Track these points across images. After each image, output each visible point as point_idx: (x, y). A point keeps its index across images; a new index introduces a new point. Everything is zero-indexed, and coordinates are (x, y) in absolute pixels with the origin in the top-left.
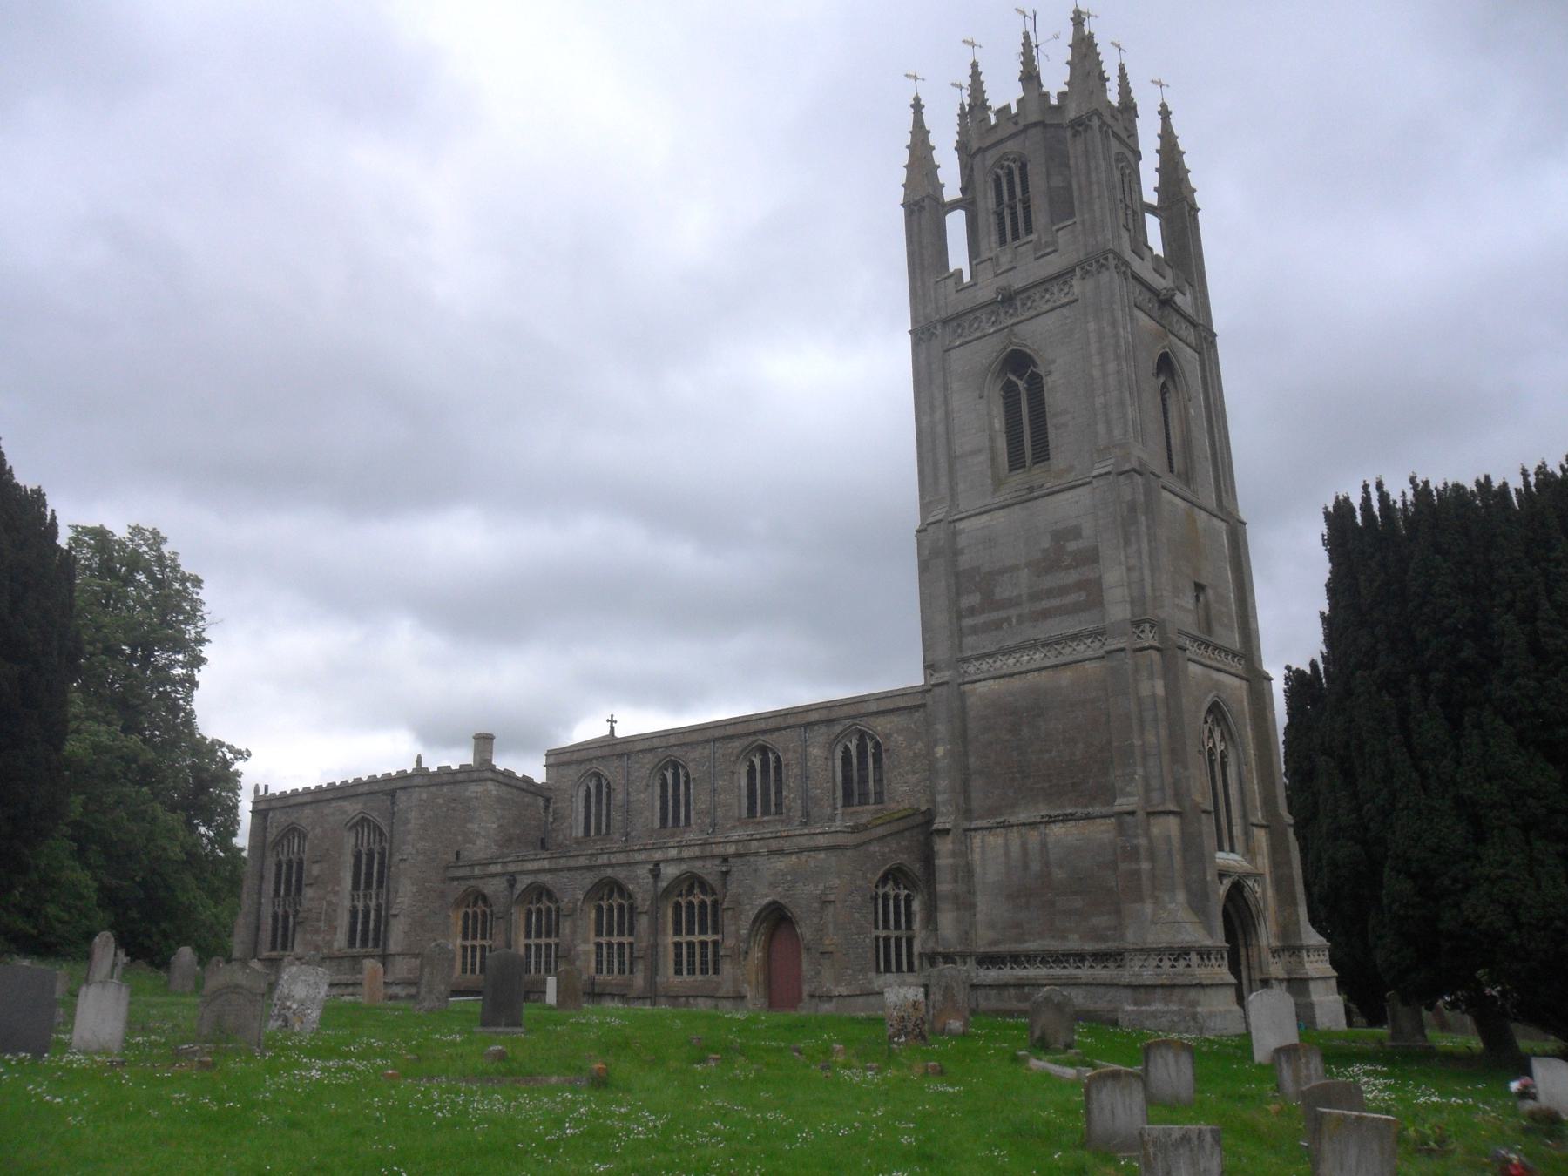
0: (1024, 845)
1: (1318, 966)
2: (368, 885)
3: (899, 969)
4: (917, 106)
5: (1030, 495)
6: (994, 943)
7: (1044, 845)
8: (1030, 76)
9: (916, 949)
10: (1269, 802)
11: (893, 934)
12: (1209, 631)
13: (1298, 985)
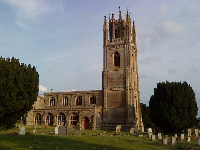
0: (114, 110)
4: (105, 17)
5: (117, 70)
8: (120, 17)
10: (139, 106)
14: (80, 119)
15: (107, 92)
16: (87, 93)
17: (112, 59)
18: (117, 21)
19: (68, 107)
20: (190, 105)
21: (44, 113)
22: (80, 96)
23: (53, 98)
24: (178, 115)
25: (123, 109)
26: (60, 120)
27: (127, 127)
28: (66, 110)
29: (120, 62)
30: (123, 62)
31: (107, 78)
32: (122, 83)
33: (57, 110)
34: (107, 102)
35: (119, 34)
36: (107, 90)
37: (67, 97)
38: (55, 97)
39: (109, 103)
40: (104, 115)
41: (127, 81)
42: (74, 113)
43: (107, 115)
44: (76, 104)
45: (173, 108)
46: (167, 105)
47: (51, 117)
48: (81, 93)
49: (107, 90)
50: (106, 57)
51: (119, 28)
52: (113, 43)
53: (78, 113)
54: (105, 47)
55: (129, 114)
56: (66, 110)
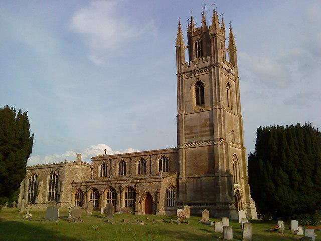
1: (253, 205)
2: (53, 188)
3: (171, 206)
4: (179, 24)
6: (191, 201)
7: (201, 182)
8: (204, 22)
9: (174, 202)
11: (170, 199)
12: (234, 140)
13: (249, 209)
14: (139, 197)
15: (183, 152)
16: (154, 153)
17: (192, 94)
18: (197, 28)
19: (125, 178)
20: (316, 165)
21: (86, 188)
22: (144, 158)
23: (104, 164)
24: (292, 186)
25: (211, 179)
26: (109, 200)
27: (217, 210)
28: (117, 182)
29: (205, 99)
30: (209, 98)
31: (185, 126)
32: (208, 133)
33: (104, 183)
34: (185, 168)
35: (202, 51)
36: (184, 147)
37: (124, 161)
38: (108, 162)
39: (188, 168)
40: (180, 190)
41: (215, 130)
42: (130, 188)
43: (186, 190)
44: (138, 172)
45: (282, 173)
46: (271, 168)
47: (97, 195)
48: (144, 154)
49: (184, 147)
50: (182, 91)
51: (201, 42)
52: (192, 68)
53: (135, 186)
54: (179, 75)
55: (220, 187)
56: (117, 182)
